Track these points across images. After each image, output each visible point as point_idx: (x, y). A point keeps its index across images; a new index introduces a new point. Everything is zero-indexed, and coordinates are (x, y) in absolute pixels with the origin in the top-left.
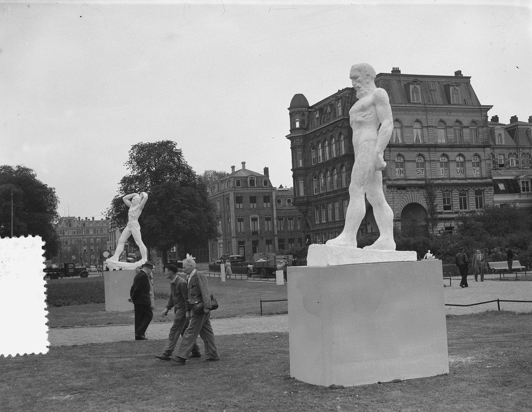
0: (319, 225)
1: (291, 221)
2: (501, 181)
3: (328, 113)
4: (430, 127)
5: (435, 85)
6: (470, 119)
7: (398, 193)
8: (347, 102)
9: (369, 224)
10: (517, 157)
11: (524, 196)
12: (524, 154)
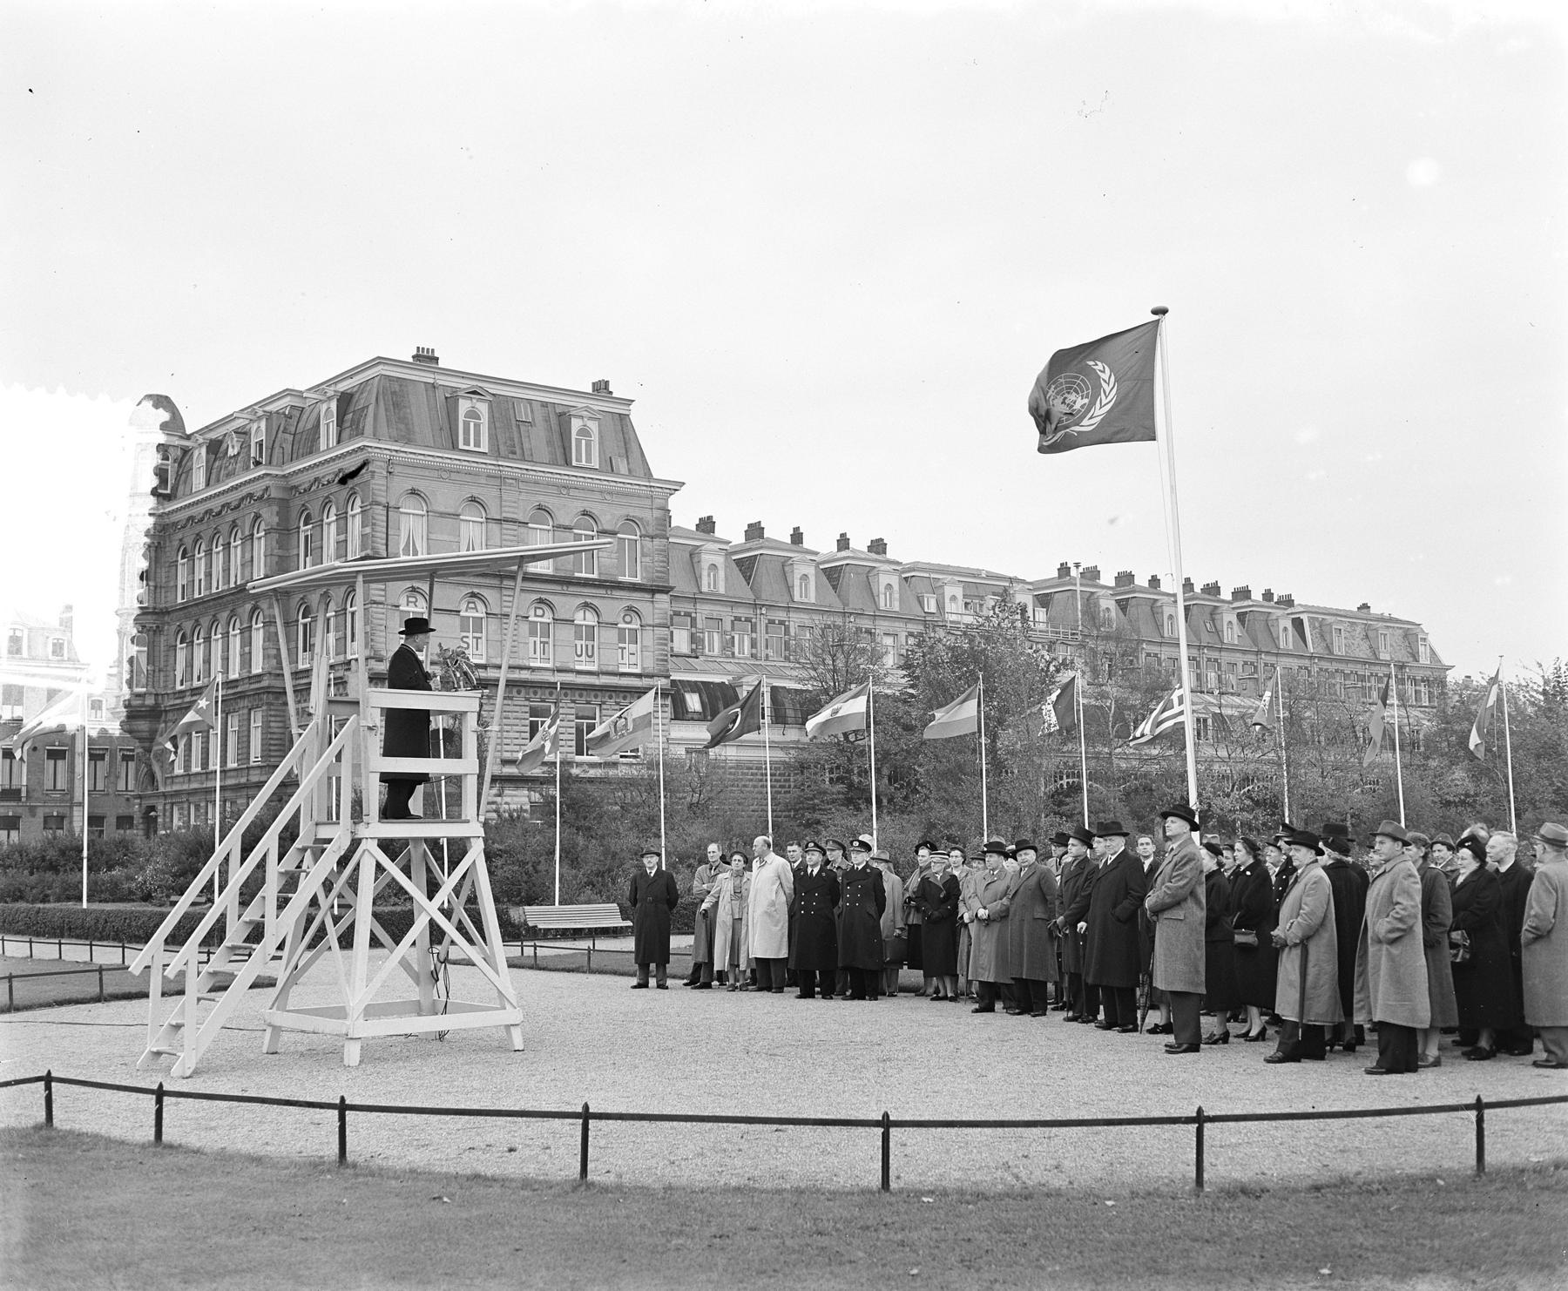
0: (181, 780)
1: (130, 763)
2: (695, 687)
3: (231, 457)
4: (506, 520)
5: (532, 411)
8: (285, 428)
10: (754, 630)
12: (772, 622)
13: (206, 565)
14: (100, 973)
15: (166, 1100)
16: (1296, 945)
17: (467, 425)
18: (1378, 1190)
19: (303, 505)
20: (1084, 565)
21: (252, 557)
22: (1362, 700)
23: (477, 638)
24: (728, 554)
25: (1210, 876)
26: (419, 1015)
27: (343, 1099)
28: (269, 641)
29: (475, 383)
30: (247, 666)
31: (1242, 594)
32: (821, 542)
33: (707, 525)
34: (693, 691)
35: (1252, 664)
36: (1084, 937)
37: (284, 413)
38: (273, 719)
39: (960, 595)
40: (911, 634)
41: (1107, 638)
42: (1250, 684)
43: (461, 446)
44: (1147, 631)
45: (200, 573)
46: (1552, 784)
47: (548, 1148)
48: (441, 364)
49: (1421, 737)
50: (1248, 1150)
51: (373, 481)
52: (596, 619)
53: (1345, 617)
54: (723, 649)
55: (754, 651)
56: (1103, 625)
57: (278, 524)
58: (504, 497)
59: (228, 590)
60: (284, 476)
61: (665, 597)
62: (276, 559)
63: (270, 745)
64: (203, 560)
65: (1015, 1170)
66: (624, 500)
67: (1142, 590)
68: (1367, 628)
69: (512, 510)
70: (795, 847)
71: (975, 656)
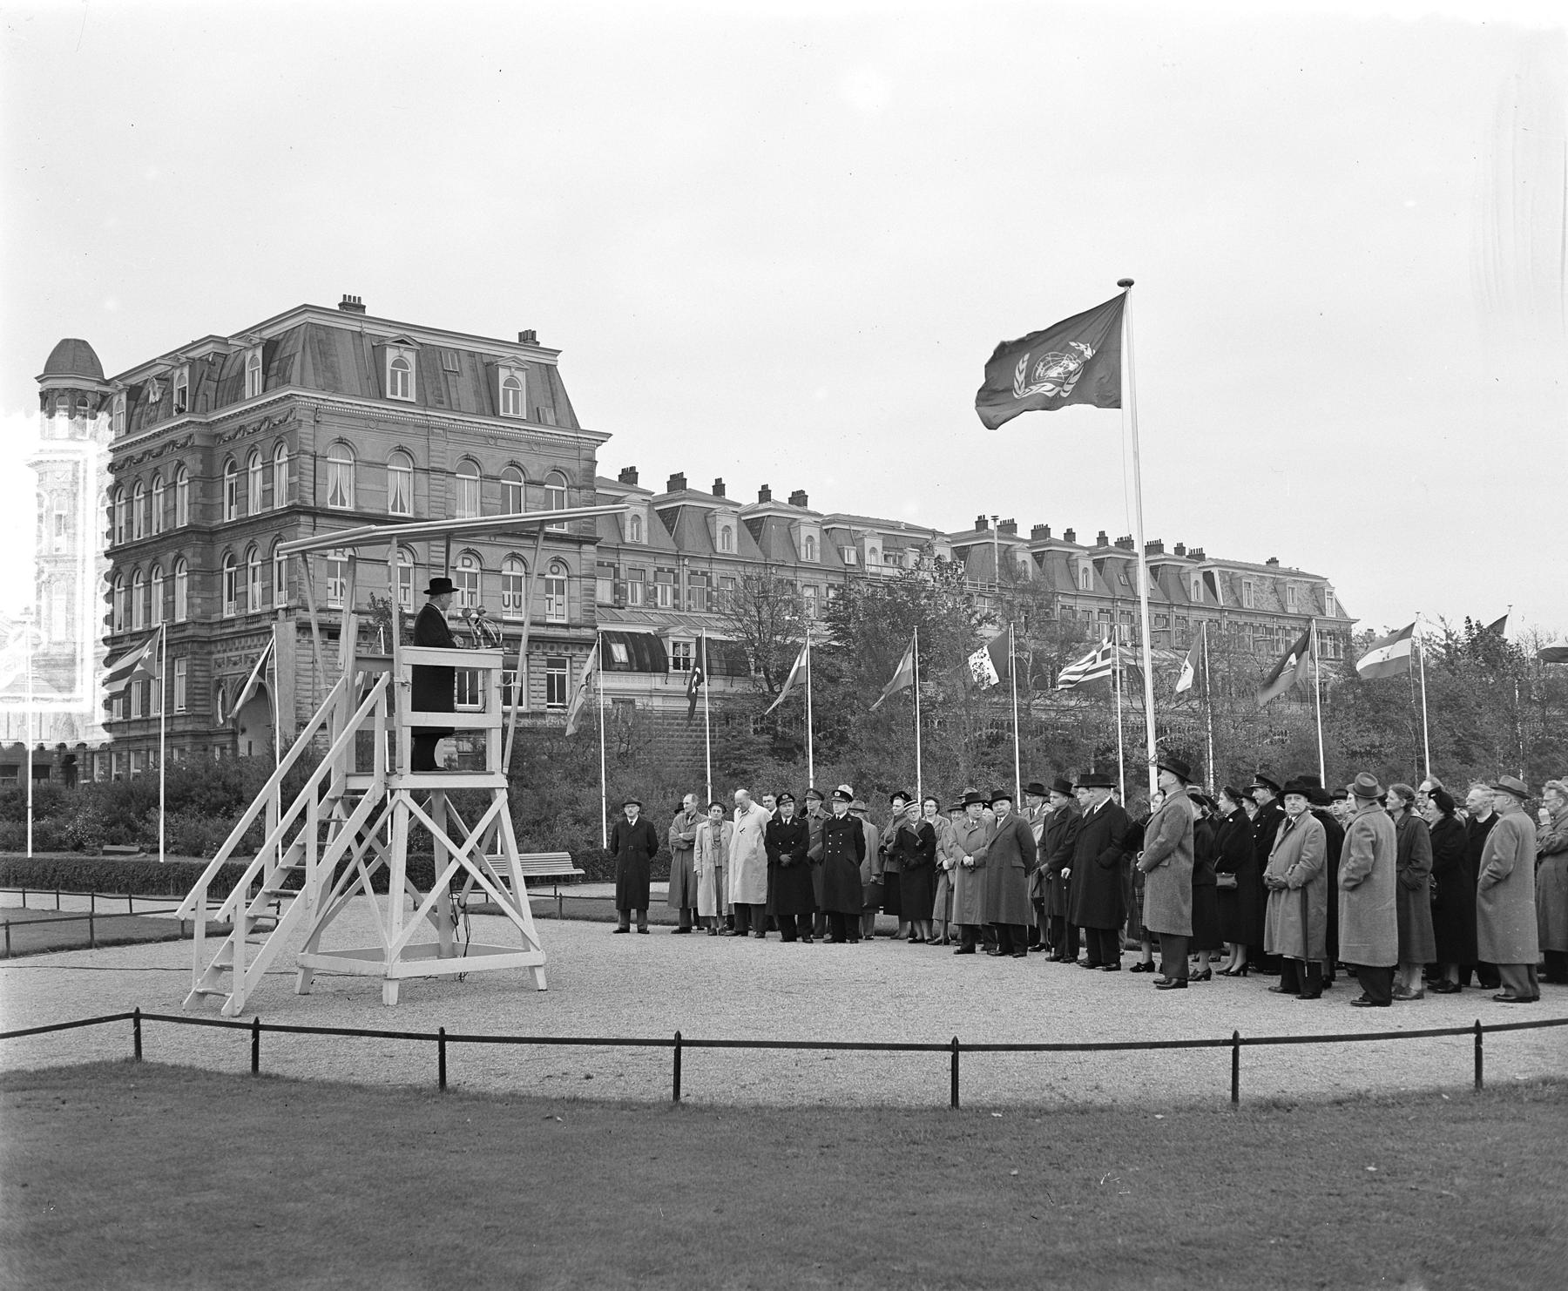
2: (621, 638)
3: (152, 404)
4: (434, 470)
5: (459, 361)
6: (548, 463)
7: (329, 647)
8: (209, 376)
9: (244, 731)
10: (676, 580)
11: (677, 681)
12: (694, 573)
13: (127, 513)
14: (91, 920)
15: (262, 1033)
16: (1297, 889)
17: (394, 373)
18: (1393, 1104)
19: (228, 453)
20: (1001, 518)
21: (175, 505)
22: (1272, 653)
23: (405, 588)
24: (651, 505)
25: (1197, 823)
26: (439, 958)
27: (442, 1030)
28: (193, 590)
29: (402, 332)
30: (170, 614)
31: (1154, 548)
32: (743, 494)
33: (629, 476)
34: (619, 642)
35: (1164, 616)
36: (1068, 882)
37: (207, 360)
38: (197, 668)
39: (879, 548)
40: (831, 586)
41: (1024, 591)
42: (1164, 637)
43: (389, 396)
44: (1061, 584)
45: (120, 519)
46: (1453, 735)
47: (621, 1075)
48: (368, 313)
49: (1328, 689)
50: (1263, 1072)
51: (302, 430)
52: (524, 570)
53: (1255, 571)
54: (646, 599)
55: (676, 602)
56: (1019, 577)
57: (202, 473)
58: (432, 447)
59: (150, 538)
60: (208, 424)
61: (592, 548)
62: (200, 507)
63: (195, 694)
64: (124, 507)
65: (1060, 1091)
66: (551, 451)
67: (1057, 543)
68: (1276, 582)
69: (438, 460)
70: (770, 797)
71: (898, 609)
